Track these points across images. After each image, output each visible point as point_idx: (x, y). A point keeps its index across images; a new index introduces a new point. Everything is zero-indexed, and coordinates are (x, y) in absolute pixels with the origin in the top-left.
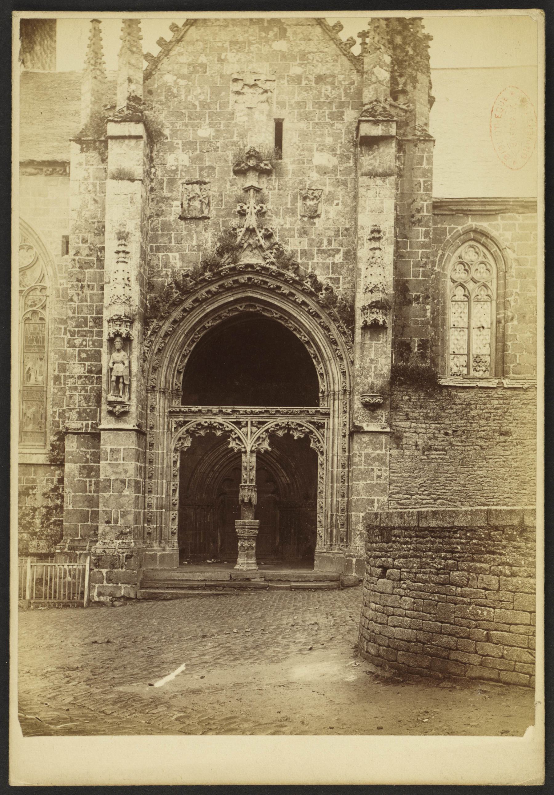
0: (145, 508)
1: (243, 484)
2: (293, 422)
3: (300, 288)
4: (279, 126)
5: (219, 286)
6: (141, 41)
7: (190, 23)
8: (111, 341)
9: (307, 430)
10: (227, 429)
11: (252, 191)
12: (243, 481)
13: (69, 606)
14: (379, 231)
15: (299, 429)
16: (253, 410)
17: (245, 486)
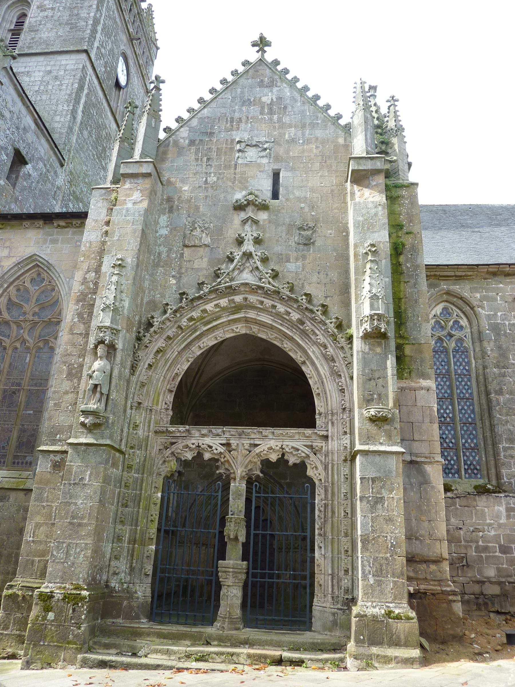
1: (230, 516)
2: (288, 446)
4: (276, 175)
6: (160, 113)
7: (323, 535)
9: (303, 455)
10: (215, 451)
11: (249, 222)
12: (230, 513)
15: (294, 453)
16: (245, 430)
17: (231, 518)
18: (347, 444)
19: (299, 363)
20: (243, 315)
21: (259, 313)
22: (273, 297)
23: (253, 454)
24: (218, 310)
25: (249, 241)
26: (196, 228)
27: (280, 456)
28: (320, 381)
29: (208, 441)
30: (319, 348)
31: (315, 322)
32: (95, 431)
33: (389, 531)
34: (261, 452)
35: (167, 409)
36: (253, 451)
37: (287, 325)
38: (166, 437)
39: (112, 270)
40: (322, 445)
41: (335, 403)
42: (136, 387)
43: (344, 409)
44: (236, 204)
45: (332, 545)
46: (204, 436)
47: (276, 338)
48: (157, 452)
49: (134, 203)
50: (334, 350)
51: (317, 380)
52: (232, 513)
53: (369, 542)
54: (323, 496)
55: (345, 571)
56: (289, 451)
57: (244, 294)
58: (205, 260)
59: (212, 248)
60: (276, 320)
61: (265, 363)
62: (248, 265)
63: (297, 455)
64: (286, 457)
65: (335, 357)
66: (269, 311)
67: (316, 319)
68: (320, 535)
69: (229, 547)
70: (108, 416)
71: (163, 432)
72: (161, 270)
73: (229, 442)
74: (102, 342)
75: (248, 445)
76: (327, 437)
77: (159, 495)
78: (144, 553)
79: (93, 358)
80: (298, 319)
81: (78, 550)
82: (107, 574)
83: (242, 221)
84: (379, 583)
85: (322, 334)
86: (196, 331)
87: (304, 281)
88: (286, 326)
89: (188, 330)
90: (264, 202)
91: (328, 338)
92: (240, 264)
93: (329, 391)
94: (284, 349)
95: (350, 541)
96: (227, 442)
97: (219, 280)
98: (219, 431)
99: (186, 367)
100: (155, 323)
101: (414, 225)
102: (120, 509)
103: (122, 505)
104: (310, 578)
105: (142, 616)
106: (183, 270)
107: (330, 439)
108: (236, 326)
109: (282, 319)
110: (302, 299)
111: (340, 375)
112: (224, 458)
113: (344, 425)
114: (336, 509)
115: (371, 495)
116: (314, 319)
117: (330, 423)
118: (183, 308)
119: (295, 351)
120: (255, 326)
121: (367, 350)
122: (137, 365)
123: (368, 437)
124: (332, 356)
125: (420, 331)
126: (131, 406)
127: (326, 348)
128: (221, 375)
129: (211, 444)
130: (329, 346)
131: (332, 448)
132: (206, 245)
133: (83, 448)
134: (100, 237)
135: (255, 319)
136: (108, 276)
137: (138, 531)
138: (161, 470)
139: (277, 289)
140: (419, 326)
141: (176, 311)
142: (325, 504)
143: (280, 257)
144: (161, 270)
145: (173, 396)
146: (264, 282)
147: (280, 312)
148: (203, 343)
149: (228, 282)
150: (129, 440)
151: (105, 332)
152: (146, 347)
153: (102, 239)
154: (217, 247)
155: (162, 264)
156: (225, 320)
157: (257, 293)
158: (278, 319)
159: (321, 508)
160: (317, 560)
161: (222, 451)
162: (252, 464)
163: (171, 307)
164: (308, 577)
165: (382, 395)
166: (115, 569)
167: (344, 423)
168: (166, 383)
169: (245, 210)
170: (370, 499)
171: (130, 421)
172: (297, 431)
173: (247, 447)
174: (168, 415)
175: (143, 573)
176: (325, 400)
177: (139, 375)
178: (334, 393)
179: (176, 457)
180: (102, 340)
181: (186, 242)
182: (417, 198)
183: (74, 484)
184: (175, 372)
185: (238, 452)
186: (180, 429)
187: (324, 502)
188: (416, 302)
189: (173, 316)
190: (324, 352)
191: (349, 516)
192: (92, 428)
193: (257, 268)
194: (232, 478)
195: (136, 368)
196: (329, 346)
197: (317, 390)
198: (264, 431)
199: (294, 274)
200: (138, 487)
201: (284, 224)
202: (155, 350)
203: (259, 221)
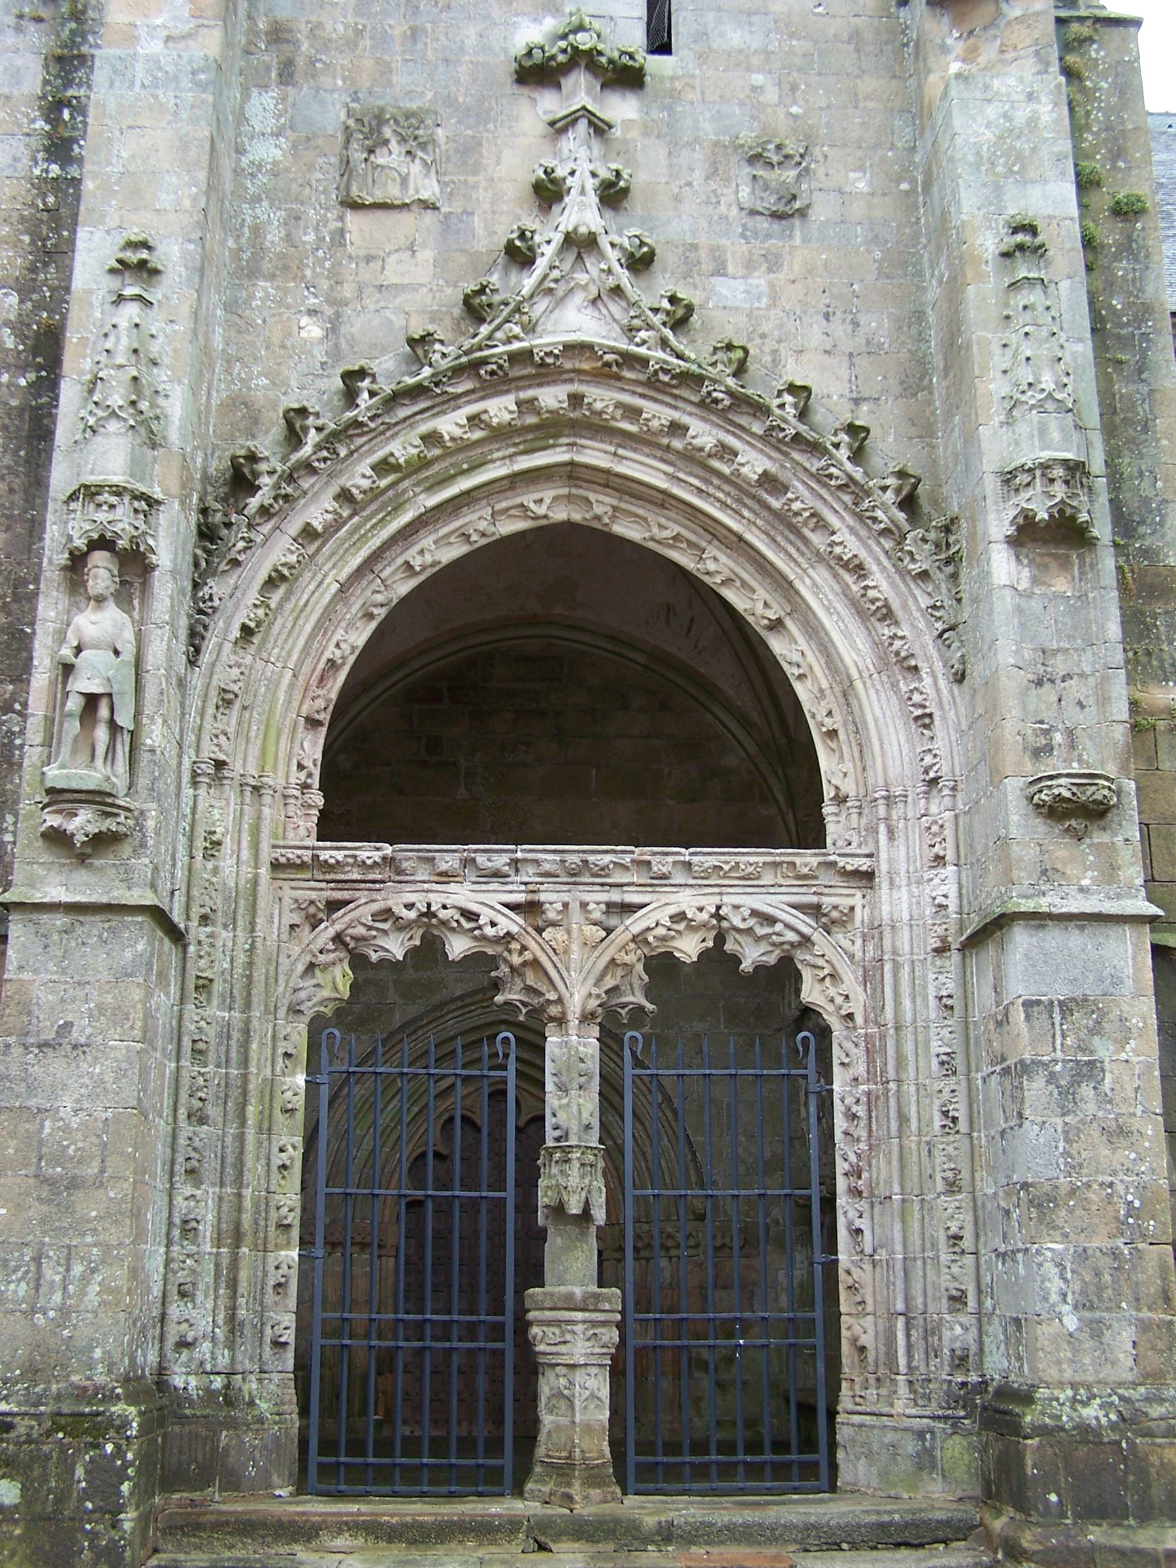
0: (222, 1184)
2: (736, 907)
3: (757, 428)
5: (470, 419)
8: (77, 562)
9: (791, 936)
10: (489, 931)
13: (33, 520)
14: (1032, 230)
15: (761, 931)
16: (592, 858)
18: (945, 896)
19: (758, 625)
20: (566, 457)
21: (621, 451)
22: (676, 397)
23: (621, 936)
24: (478, 435)
25: (583, 192)
26: (386, 142)
27: (710, 944)
28: (837, 689)
29: (462, 894)
30: (836, 576)
31: (826, 486)
32: (98, 863)
33: (1119, 1167)
34: (649, 929)
35: (305, 786)
36: (621, 928)
37: (721, 495)
38: (313, 884)
39: (114, 283)
40: (850, 902)
41: (898, 763)
42: (203, 708)
43: (934, 781)
44: (528, 63)
45: (903, 1221)
46: (446, 877)
47: (677, 537)
48: (285, 937)
49: (169, 39)
50: (892, 584)
51: (825, 685)
52: (557, 1133)
53: (1057, 1206)
54: (861, 1069)
55: (952, 1298)
56: (742, 926)
57: (571, 381)
58: (427, 255)
59: (448, 216)
60: (681, 475)
61: (554, 631)
62: (581, 277)
63: (768, 936)
64: (729, 947)
65: (895, 605)
66: (659, 446)
67: (830, 476)
68: (856, 1193)
69: (554, 1243)
70: (144, 807)
71: (303, 866)
72: (265, 289)
73: (535, 897)
74: (103, 543)
75: (603, 907)
76: (867, 877)
77: (300, 1079)
78: (265, 1273)
79: (64, 601)
80: (765, 473)
81: (78, 1269)
82: (157, 1347)
83: (552, 124)
84: (1096, 1329)
85: (852, 530)
86: (398, 508)
87: (779, 342)
88: (719, 500)
89: (374, 507)
90: (625, 60)
91: (870, 542)
92: (556, 274)
93: (876, 721)
94: (707, 579)
95: (967, 1204)
96: (530, 897)
97: (484, 330)
98: (501, 861)
99: (361, 636)
100: (265, 480)
101: (1130, 168)
102: (186, 1130)
103: (189, 1116)
105: (275, 1479)
106: (348, 291)
107: (882, 880)
108: (538, 496)
109: (702, 473)
110: (782, 406)
111: (916, 668)
112: (520, 954)
113: (935, 835)
114: (914, 1108)
115: (1059, 1055)
116: (822, 477)
117: (882, 828)
118: (361, 425)
119: (744, 583)
120: (602, 498)
121: (1024, 585)
122: (206, 627)
123: (1044, 872)
124: (887, 605)
125: (1162, 524)
126: (194, 775)
127: (864, 577)
128: (402, 673)
129: (474, 907)
130: (875, 568)
131: (891, 913)
132: (428, 206)
133: (60, 920)
134: (26, 161)
135: (608, 472)
136: (96, 303)
137: (248, 1203)
138: (303, 995)
139: (694, 368)
140: (1159, 510)
141: (335, 436)
142: (869, 1094)
143: (692, 255)
144: (263, 288)
145: (322, 741)
146: (644, 342)
147: (701, 449)
148: (422, 552)
149: (516, 337)
150: (195, 892)
151: (112, 507)
153: (37, 172)
154: (465, 212)
155: (266, 266)
157: (619, 378)
158: (690, 474)
159: (855, 1109)
160: (848, 1272)
161: (515, 929)
162: (620, 972)
163: (320, 422)
164: (819, 1324)
165: (1078, 732)
166: (185, 1326)
167: (935, 828)
168: (297, 695)
169: (558, 86)
170: (1058, 1068)
171: (192, 826)
172: (769, 859)
173: (597, 915)
174: (310, 806)
175: (267, 1340)
176: (857, 755)
177: (213, 665)
178: (892, 730)
179: (350, 952)
180: (102, 536)
181: (355, 191)
182: (1137, 71)
183: (39, 1046)
184: (328, 655)
185: (569, 932)
186: (363, 855)
187: (865, 1087)
188: (1146, 429)
189: (325, 454)
190: (855, 588)
191: (963, 1126)
192: (89, 850)
193: (617, 291)
194: (552, 1019)
195: (203, 638)
196: (875, 568)
197: (827, 721)
198: (658, 858)
199: (744, 319)
200: (234, 1054)
201: (697, 140)
202: (263, 576)
203: (610, 127)
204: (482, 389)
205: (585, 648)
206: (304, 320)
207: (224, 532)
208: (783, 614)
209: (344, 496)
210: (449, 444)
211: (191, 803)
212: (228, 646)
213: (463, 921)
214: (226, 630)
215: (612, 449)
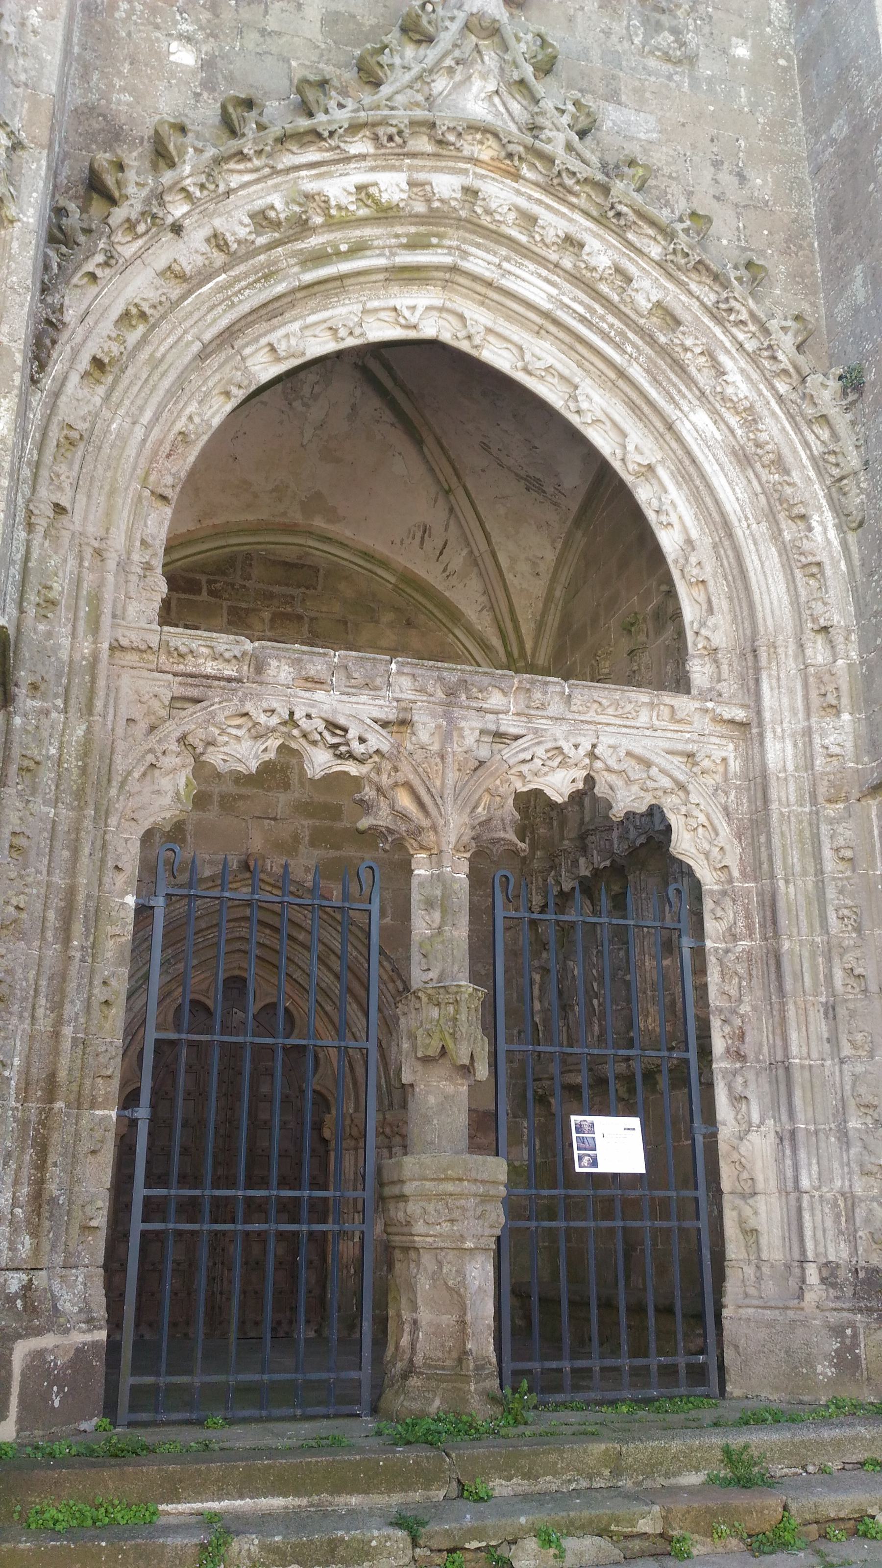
5: (360, 188)
20: (448, 260)
24: (363, 212)
46: (315, 682)
60: (566, 300)
61: (311, 543)
85: (742, 371)
100: (131, 190)
104: (128, 1207)
108: (411, 302)
147: (594, 269)
152: (93, 277)
156: (382, 262)
184: (180, 425)
204: (375, 156)
205: (339, 560)
206: (174, 46)
207: (82, 239)
208: (654, 460)
209: (217, 240)
210: (333, 212)
211: (23, 550)
212: (74, 379)
213: (327, 734)
214: (73, 359)
215: (497, 261)
